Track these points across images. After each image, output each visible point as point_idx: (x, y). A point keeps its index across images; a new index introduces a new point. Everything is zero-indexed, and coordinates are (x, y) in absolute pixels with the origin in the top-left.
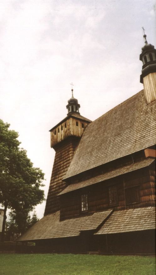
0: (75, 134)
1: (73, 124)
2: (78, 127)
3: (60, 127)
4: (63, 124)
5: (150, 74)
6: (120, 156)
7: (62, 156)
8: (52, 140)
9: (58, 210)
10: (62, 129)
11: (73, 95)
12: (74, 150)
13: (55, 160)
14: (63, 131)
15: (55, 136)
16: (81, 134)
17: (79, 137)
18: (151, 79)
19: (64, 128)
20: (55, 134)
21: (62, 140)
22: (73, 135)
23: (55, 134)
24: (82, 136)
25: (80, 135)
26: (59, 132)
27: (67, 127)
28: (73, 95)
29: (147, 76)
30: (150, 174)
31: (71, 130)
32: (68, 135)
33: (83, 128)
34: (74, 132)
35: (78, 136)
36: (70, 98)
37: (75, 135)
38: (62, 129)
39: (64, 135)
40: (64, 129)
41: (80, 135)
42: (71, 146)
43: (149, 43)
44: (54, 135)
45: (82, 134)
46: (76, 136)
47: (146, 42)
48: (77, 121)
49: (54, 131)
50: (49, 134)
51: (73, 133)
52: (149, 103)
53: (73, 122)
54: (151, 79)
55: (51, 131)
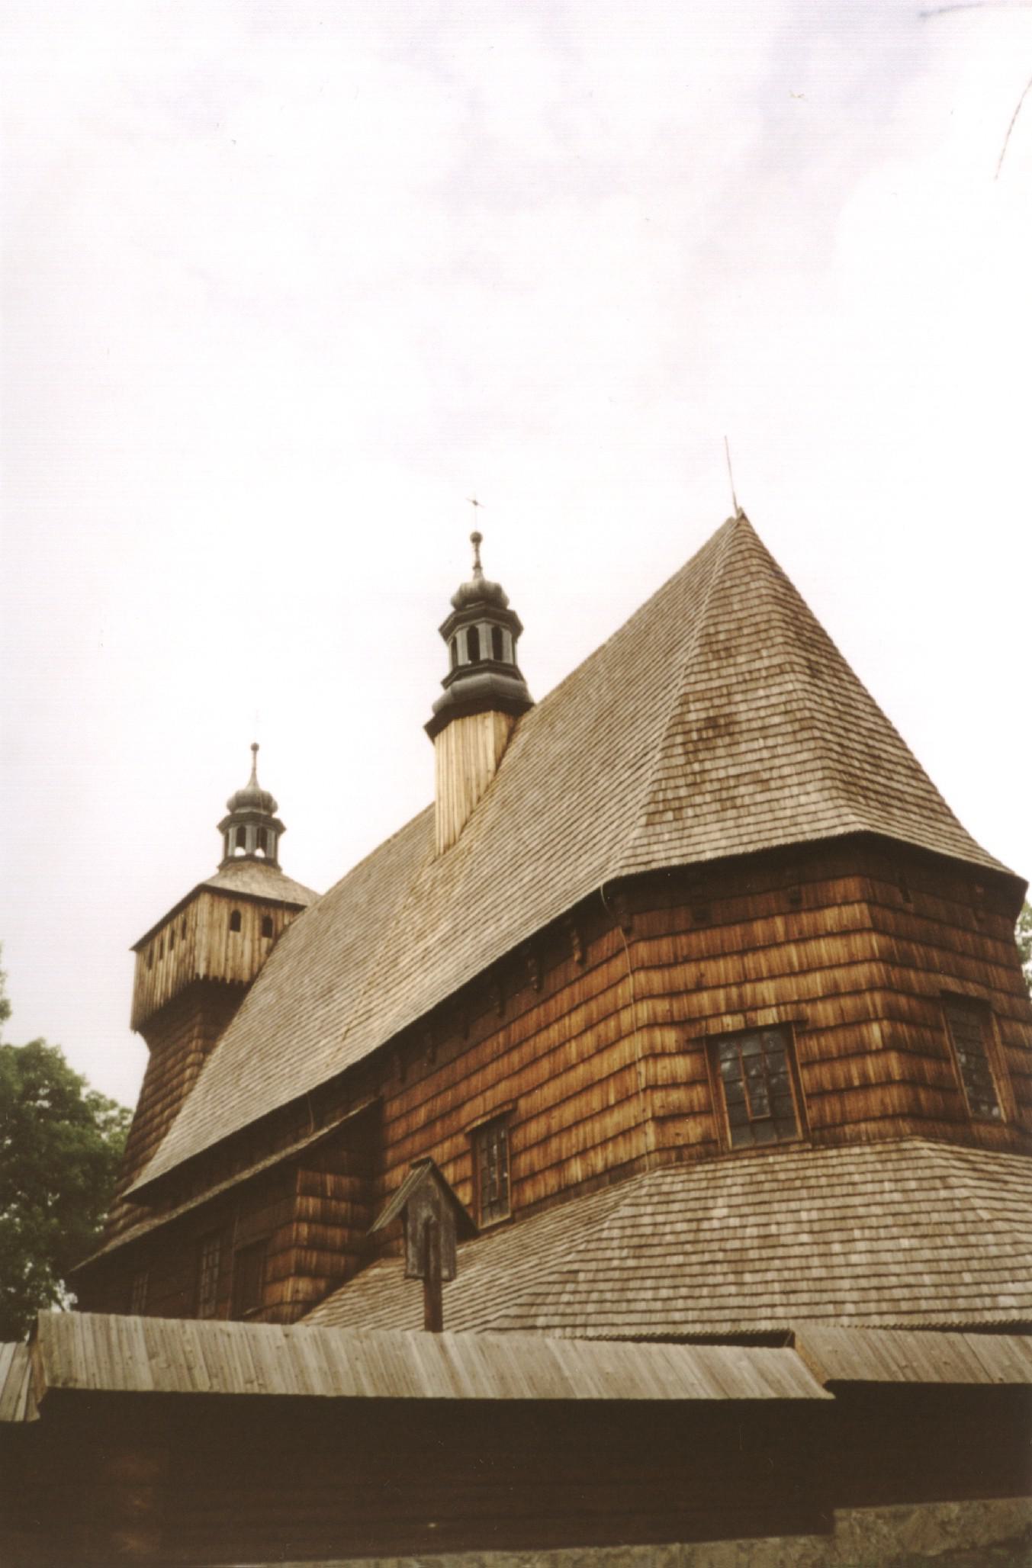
0: (218, 970)
1: (211, 926)
2: (239, 935)
3: (167, 933)
4: (178, 922)
5: (492, 713)
6: (284, 1095)
7: (164, 1074)
8: (136, 995)
9: (835, 1393)
10: (172, 946)
11: (254, 769)
12: (207, 1051)
13: (143, 1091)
14: (173, 952)
15: (148, 975)
16: (251, 969)
17: (241, 982)
18: (453, 745)
19: (177, 940)
20: (150, 965)
21: (166, 1000)
22: (206, 976)
23: (150, 965)
24: (254, 977)
25: (246, 976)
26: (161, 956)
27: (189, 935)
28: (254, 769)
29: (445, 731)
30: (298, 1191)
31: (201, 954)
32: (186, 975)
33: (265, 941)
34: (214, 965)
35: (232, 980)
36: (240, 784)
37: (215, 978)
38: (172, 946)
39: (175, 974)
40: (181, 945)
41: (246, 976)
42: (196, 1031)
43: (491, 576)
44: (145, 969)
45: (256, 970)
46: (224, 979)
47: (478, 566)
48: (233, 907)
49: (148, 953)
50: (129, 962)
51: (208, 966)
52: (439, 854)
53: (211, 913)
54: (453, 745)
55: (139, 947)
